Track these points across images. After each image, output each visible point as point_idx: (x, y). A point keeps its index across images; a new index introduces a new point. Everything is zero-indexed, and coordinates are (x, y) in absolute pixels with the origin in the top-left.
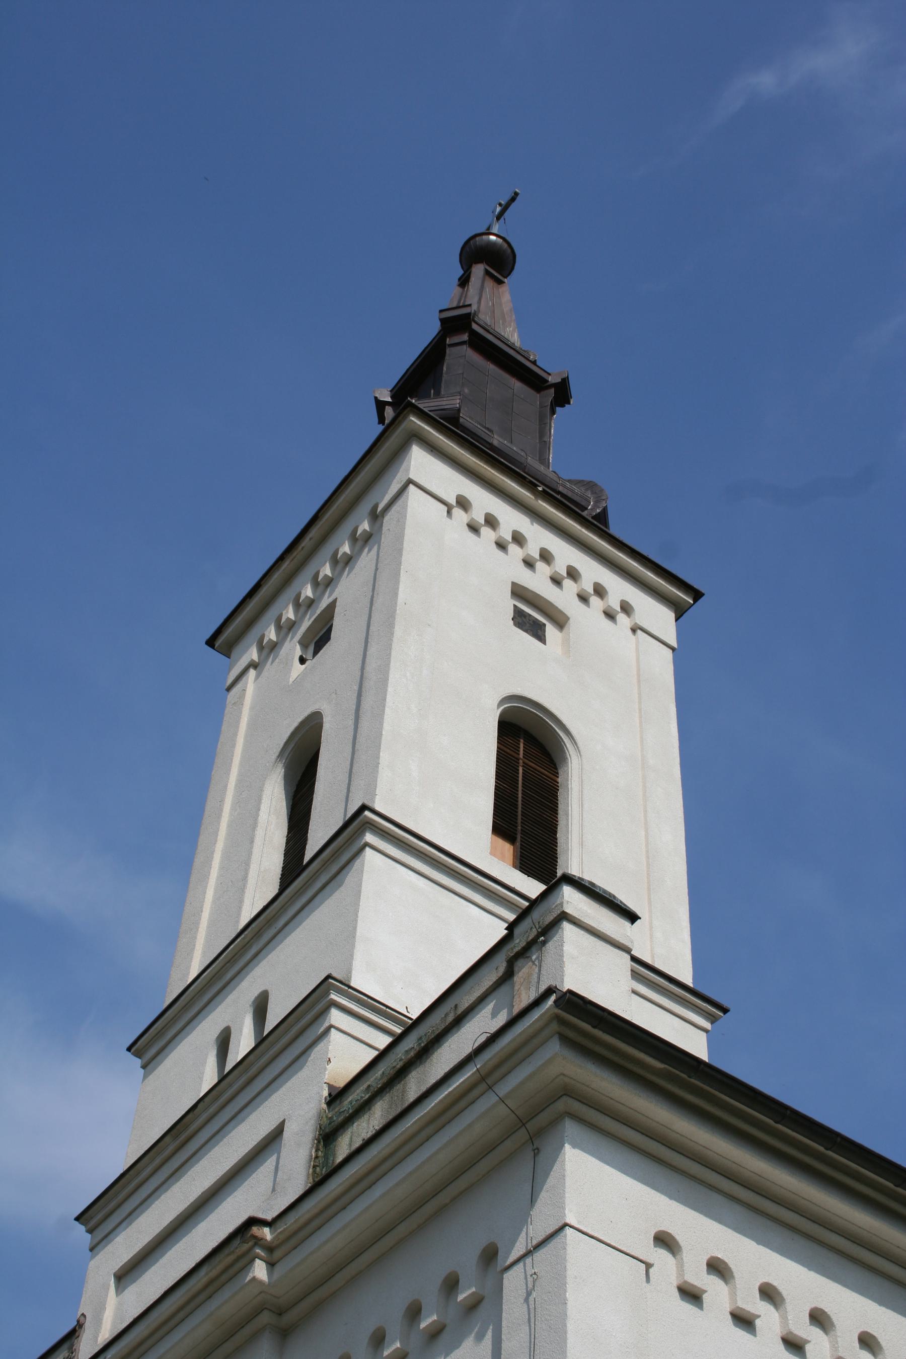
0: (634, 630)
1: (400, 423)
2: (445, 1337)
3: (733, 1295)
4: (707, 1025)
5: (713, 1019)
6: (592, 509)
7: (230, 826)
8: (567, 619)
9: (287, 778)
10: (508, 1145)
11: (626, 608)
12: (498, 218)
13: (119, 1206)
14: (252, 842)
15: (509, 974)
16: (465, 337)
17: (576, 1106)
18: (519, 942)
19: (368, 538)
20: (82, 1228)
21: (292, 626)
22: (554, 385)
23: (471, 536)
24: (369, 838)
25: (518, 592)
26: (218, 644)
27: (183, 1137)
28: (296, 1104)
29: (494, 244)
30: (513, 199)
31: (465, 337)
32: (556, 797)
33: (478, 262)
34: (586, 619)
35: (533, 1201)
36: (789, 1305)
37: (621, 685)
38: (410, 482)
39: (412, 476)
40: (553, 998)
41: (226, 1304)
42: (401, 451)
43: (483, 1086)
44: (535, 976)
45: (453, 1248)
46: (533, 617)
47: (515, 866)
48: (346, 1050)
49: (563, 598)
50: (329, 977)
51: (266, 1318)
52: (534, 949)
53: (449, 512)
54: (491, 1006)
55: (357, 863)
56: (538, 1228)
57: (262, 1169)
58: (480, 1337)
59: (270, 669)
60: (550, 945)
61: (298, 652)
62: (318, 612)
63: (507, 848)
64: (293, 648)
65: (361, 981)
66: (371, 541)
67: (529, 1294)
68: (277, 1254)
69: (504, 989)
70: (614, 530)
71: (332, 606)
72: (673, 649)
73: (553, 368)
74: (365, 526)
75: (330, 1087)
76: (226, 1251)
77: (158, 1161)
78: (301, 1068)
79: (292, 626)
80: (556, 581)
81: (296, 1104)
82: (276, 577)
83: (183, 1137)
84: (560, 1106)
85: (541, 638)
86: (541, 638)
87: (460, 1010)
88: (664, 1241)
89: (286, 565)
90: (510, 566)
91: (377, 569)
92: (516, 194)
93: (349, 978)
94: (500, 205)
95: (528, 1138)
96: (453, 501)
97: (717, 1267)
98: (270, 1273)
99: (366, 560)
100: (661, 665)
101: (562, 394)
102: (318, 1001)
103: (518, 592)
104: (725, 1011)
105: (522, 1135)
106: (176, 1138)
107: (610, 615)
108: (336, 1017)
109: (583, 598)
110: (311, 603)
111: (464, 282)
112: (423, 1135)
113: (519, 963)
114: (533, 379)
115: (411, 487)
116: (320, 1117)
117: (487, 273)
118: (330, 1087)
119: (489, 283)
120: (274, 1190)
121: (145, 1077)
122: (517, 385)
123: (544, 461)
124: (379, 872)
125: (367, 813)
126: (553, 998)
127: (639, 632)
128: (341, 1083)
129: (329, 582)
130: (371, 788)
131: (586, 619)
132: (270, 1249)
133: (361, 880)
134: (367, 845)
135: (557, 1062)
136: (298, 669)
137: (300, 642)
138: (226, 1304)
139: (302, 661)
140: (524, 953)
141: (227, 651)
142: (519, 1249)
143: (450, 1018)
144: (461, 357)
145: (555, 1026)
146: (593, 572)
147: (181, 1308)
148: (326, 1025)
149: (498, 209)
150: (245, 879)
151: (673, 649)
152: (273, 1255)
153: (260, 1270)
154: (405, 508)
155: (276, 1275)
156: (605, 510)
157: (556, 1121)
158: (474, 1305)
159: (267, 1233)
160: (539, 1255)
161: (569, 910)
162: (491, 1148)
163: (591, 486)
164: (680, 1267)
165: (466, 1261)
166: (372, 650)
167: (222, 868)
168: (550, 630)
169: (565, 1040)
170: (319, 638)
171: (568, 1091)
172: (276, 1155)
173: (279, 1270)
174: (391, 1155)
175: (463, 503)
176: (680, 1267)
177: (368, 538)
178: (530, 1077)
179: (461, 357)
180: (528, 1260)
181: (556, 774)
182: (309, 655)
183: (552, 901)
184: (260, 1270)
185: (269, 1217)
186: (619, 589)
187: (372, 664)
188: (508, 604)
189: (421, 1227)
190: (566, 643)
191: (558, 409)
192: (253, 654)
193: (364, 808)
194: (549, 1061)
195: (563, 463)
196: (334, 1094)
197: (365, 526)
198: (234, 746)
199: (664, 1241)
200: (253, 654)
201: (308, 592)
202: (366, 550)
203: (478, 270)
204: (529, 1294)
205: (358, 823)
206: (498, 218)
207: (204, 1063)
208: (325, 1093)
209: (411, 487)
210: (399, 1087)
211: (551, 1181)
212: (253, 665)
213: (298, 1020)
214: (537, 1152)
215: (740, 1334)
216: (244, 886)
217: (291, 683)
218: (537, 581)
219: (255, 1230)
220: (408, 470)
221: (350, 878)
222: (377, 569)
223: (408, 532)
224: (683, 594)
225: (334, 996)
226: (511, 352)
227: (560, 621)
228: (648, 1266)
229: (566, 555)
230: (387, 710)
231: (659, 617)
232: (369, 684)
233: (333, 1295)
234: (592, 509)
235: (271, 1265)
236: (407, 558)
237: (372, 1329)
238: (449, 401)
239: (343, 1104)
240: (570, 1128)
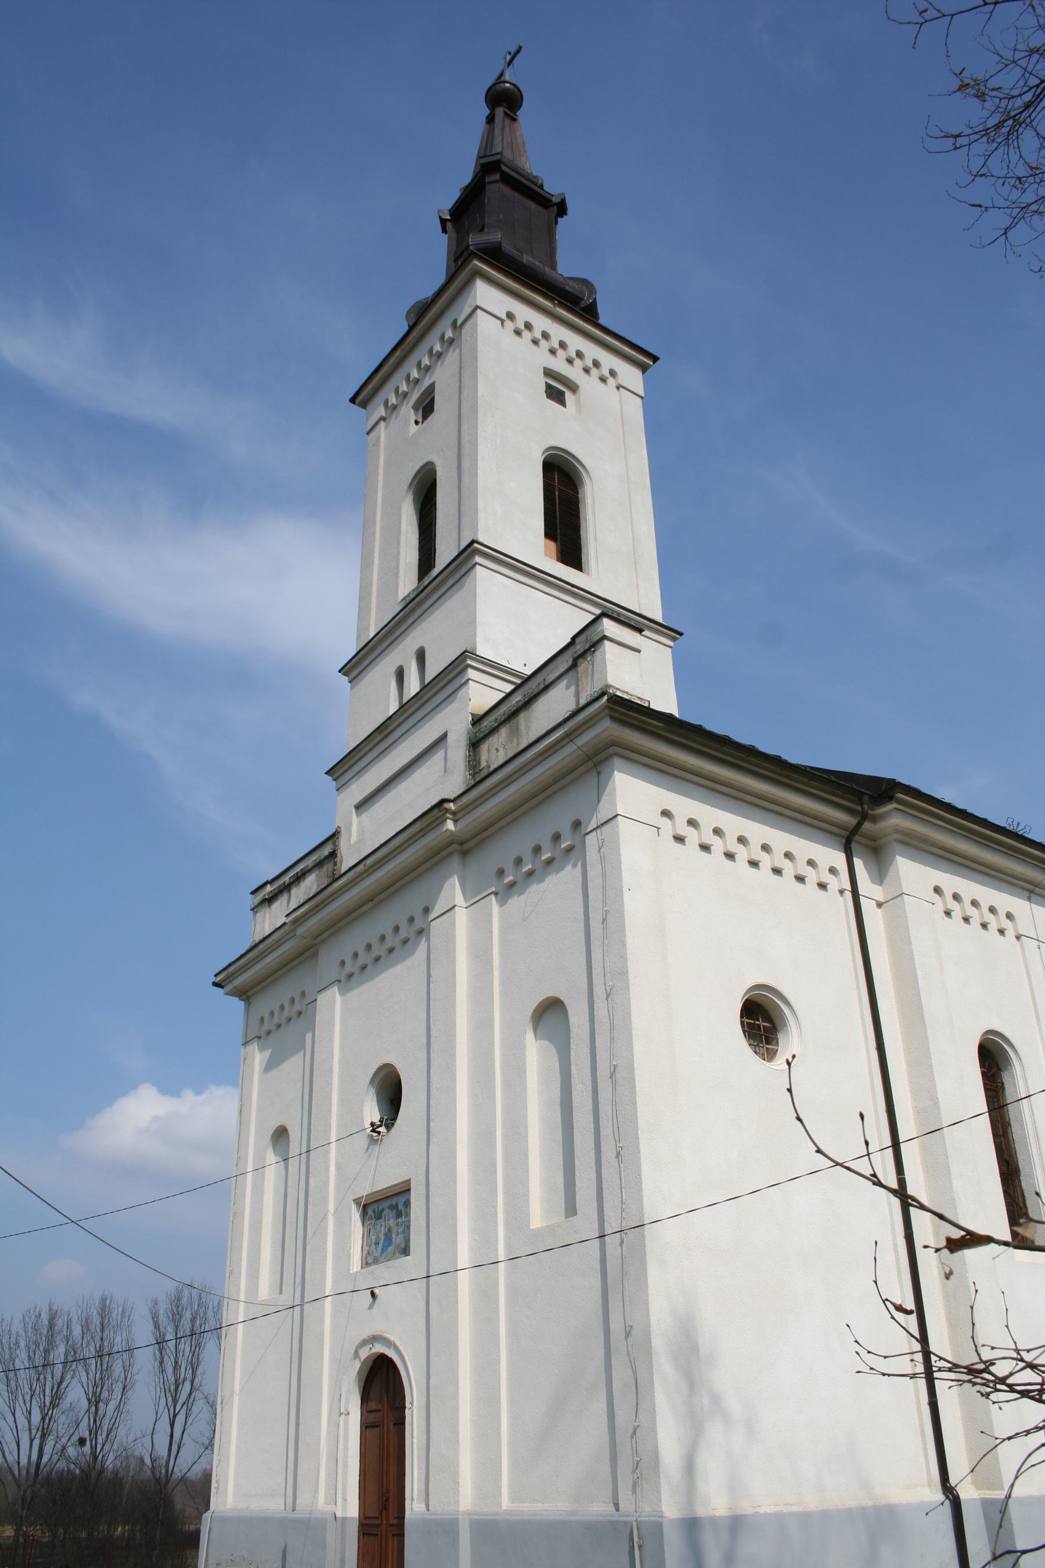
0: (618, 388)
1: (468, 264)
2: (555, 863)
3: (700, 836)
4: (671, 643)
5: (674, 639)
6: (587, 300)
7: (381, 530)
8: (578, 387)
9: (415, 500)
10: (583, 768)
11: (613, 373)
12: (509, 64)
13: (351, 767)
14: (399, 544)
15: (574, 665)
16: (497, 177)
17: (619, 750)
18: (579, 648)
19: (451, 341)
20: (330, 778)
21: (405, 395)
22: (557, 204)
23: (516, 338)
24: (478, 559)
25: (548, 373)
26: (357, 401)
27: (385, 733)
28: (453, 721)
29: (506, 90)
30: (518, 51)
31: (497, 177)
32: (578, 508)
33: (499, 105)
34: (588, 384)
35: (599, 801)
36: (727, 837)
37: (611, 430)
38: (477, 307)
39: (479, 304)
40: (606, 697)
41: (431, 839)
42: (469, 282)
43: (567, 740)
44: (590, 671)
45: (557, 817)
46: (557, 390)
47: (558, 560)
48: (482, 693)
49: (574, 373)
50: (465, 651)
51: (455, 847)
52: (588, 654)
53: (502, 324)
54: (565, 682)
55: (472, 574)
56: (602, 815)
57: (436, 756)
58: (575, 866)
59: (395, 422)
60: (597, 653)
61: (413, 417)
62: (423, 389)
63: (552, 545)
64: (408, 412)
65: (482, 651)
66: (454, 344)
67: (600, 849)
68: (458, 816)
69: (572, 673)
70: (601, 321)
71: (432, 387)
72: (642, 398)
73: (552, 187)
74: (449, 334)
75: (473, 715)
76: (430, 815)
77: (371, 745)
78: (453, 701)
79: (405, 395)
80: (570, 361)
81: (453, 721)
82: (392, 361)
83: (385, 733)
84: (611, 750)
85: (562, 402)
86: (562, 402)
87: (547, 682)
88: (666, 813)
89: (398, 353)
90: (542, 358)
91: (461, 368)
92: (520, 48)
93: (475, 649)
94: (510, 53)
95: (595, 763)
96: (504, 317)
97: (692, 823)
98: (455, 826)
99: (452, 357)
100: (635, 408)
101: (562, 209)
102: (459, 665)
103: (548, 373)
104: (681, 634)
105: (590, 764)
106: (380, 733)
107: (603, 380)
108: (471, 673)
109: (587, 370)
110: (417, 381)
111: (490, 120)
112: (536, 762)
113: (580, 661)
114: (543, 200)
115: (479, 311)
116: (469, 732)
117: (506, 114)
118: (473, 715)
119: (507, 122)
120: (445, 771)
121: (352, 688)
122: (532, 205)
123: (553, 266)
124: (485, 578)
125: (475, 545)
126: (606, 697)
127: (621, 389)
128: (481, 712)
129: (428, 369)
130: (475, 528)
131: (588, 384)
132: (454, 813)
133: (475, 586)
134: (477, 563)
135: (607, 728)
136: (414, 428)
137: (415, 408)
138: (431, 839)
139: (417, 423)
140: (583, 655)
141: (364, 405)
142: (593, 825)
143: (542, 686)
144: (496, 190)
145: (607, 711)
146: (592, 351)
147: (406, 841)
148: (466, 678)
149: (509, 57)
150: (397, 567)
151: (642, 398)
152: (456, 817)
153: (450, 825)
154: (476, 325)
155: (458, 828)
156: (595, 301)
157: (609, 757)
158: (570, 850)
159: (452, 806)
160: (605, 828)
161: (607, 634)
162: (573, 769)
163: (585, 282)
164: (674, 826)
165: (564, 826)
166: (465, 427)
167: (380, 558)
168: (568, 396)
169: (613, 719)
170: (426, 407)
171: (614, 743)
172: (443, 751)
173: (462, 824)
174: (520, 769)
175: (510, 316)
176: (674, 826)
177: (451, 341)
178: (596, 736)
179: (496, 190)
180: (599, 831)
181: (577, 493)
182: (420, 420)
183: (597, 627)
184: (450, 825)
185: (452, 797)
186: (609, 361)
187: (465, 439)
188: (541, 382)
189: (536, 806)
190: (578, 403)
191: (559, 219)
192: (382, 411)
193: (473, 542)
194: (606, 730)
195: (568, 265)
196: (476, 719)
197: (449, 334)
198: (377, 475)
199: (666, 813)
200: (382, 411)
201: (415, 374)
202: (451, 350)
203: (500, 112)
204: (600, 849)
205: (469, 553)
206: (509, 64)
207: (389, 686)
208: (470, 719)
209: (479, 311)
210: (514, 721)
211: (608, 790)
212: (383, 419)
213: (449, 673)
214: (599, 773)
215: (704, 854)
216: (397, 574)
217: (411, 435)
218: (558, 364)
219: (446, 805)
220: (475, 298)
221: (468, 582)
222: (461, 368)
223: (479, 344)
224: (644, 358)
225: (469, 662)
226: (528, 183)
227: (574, 388)
228: (658, 829)
229: (575, 342)
230: (479, 472)
231: (631, 376)
232: (465, 451)
233: (489, 836)
234: (587, 300)
235: (455, 821)
236: (481, 364)
237: (515, 856)
238: (494, 236)
239: (483, 728)
240: (617, 762)
